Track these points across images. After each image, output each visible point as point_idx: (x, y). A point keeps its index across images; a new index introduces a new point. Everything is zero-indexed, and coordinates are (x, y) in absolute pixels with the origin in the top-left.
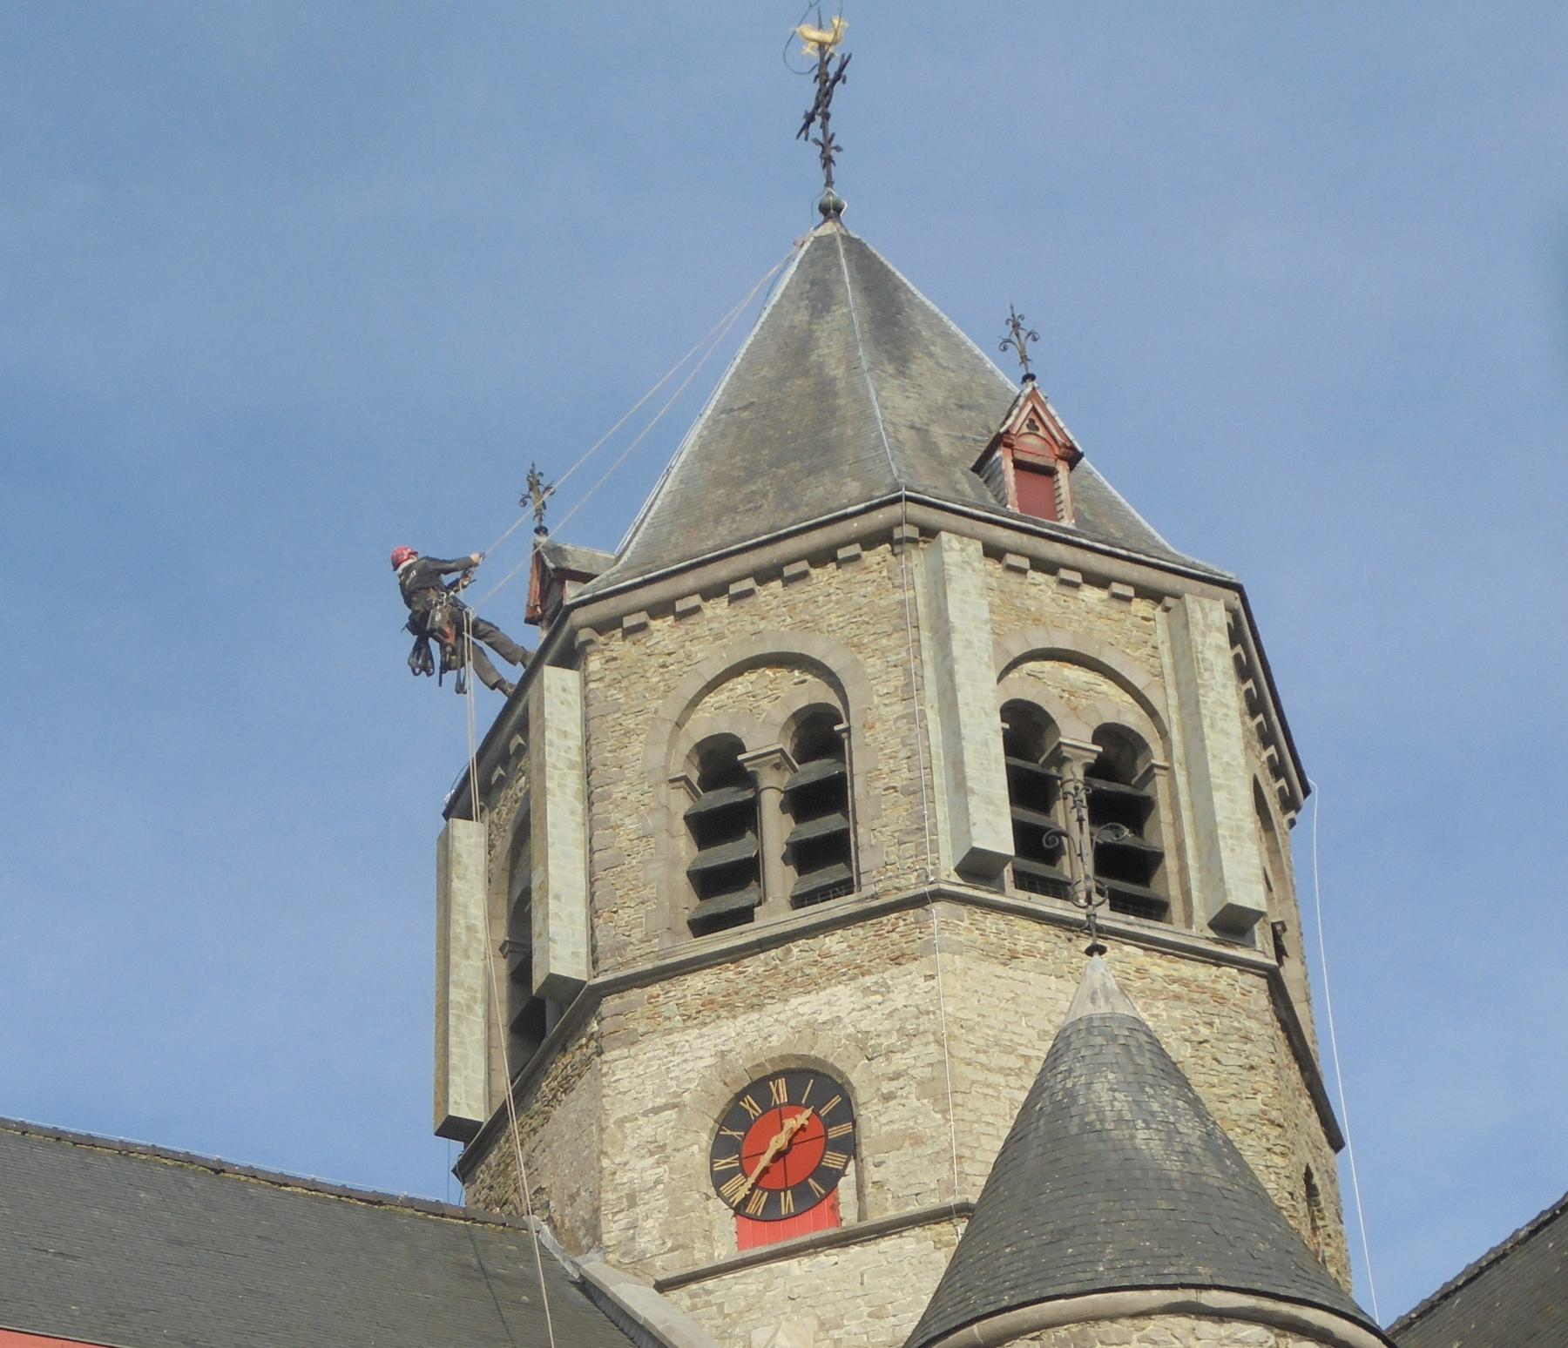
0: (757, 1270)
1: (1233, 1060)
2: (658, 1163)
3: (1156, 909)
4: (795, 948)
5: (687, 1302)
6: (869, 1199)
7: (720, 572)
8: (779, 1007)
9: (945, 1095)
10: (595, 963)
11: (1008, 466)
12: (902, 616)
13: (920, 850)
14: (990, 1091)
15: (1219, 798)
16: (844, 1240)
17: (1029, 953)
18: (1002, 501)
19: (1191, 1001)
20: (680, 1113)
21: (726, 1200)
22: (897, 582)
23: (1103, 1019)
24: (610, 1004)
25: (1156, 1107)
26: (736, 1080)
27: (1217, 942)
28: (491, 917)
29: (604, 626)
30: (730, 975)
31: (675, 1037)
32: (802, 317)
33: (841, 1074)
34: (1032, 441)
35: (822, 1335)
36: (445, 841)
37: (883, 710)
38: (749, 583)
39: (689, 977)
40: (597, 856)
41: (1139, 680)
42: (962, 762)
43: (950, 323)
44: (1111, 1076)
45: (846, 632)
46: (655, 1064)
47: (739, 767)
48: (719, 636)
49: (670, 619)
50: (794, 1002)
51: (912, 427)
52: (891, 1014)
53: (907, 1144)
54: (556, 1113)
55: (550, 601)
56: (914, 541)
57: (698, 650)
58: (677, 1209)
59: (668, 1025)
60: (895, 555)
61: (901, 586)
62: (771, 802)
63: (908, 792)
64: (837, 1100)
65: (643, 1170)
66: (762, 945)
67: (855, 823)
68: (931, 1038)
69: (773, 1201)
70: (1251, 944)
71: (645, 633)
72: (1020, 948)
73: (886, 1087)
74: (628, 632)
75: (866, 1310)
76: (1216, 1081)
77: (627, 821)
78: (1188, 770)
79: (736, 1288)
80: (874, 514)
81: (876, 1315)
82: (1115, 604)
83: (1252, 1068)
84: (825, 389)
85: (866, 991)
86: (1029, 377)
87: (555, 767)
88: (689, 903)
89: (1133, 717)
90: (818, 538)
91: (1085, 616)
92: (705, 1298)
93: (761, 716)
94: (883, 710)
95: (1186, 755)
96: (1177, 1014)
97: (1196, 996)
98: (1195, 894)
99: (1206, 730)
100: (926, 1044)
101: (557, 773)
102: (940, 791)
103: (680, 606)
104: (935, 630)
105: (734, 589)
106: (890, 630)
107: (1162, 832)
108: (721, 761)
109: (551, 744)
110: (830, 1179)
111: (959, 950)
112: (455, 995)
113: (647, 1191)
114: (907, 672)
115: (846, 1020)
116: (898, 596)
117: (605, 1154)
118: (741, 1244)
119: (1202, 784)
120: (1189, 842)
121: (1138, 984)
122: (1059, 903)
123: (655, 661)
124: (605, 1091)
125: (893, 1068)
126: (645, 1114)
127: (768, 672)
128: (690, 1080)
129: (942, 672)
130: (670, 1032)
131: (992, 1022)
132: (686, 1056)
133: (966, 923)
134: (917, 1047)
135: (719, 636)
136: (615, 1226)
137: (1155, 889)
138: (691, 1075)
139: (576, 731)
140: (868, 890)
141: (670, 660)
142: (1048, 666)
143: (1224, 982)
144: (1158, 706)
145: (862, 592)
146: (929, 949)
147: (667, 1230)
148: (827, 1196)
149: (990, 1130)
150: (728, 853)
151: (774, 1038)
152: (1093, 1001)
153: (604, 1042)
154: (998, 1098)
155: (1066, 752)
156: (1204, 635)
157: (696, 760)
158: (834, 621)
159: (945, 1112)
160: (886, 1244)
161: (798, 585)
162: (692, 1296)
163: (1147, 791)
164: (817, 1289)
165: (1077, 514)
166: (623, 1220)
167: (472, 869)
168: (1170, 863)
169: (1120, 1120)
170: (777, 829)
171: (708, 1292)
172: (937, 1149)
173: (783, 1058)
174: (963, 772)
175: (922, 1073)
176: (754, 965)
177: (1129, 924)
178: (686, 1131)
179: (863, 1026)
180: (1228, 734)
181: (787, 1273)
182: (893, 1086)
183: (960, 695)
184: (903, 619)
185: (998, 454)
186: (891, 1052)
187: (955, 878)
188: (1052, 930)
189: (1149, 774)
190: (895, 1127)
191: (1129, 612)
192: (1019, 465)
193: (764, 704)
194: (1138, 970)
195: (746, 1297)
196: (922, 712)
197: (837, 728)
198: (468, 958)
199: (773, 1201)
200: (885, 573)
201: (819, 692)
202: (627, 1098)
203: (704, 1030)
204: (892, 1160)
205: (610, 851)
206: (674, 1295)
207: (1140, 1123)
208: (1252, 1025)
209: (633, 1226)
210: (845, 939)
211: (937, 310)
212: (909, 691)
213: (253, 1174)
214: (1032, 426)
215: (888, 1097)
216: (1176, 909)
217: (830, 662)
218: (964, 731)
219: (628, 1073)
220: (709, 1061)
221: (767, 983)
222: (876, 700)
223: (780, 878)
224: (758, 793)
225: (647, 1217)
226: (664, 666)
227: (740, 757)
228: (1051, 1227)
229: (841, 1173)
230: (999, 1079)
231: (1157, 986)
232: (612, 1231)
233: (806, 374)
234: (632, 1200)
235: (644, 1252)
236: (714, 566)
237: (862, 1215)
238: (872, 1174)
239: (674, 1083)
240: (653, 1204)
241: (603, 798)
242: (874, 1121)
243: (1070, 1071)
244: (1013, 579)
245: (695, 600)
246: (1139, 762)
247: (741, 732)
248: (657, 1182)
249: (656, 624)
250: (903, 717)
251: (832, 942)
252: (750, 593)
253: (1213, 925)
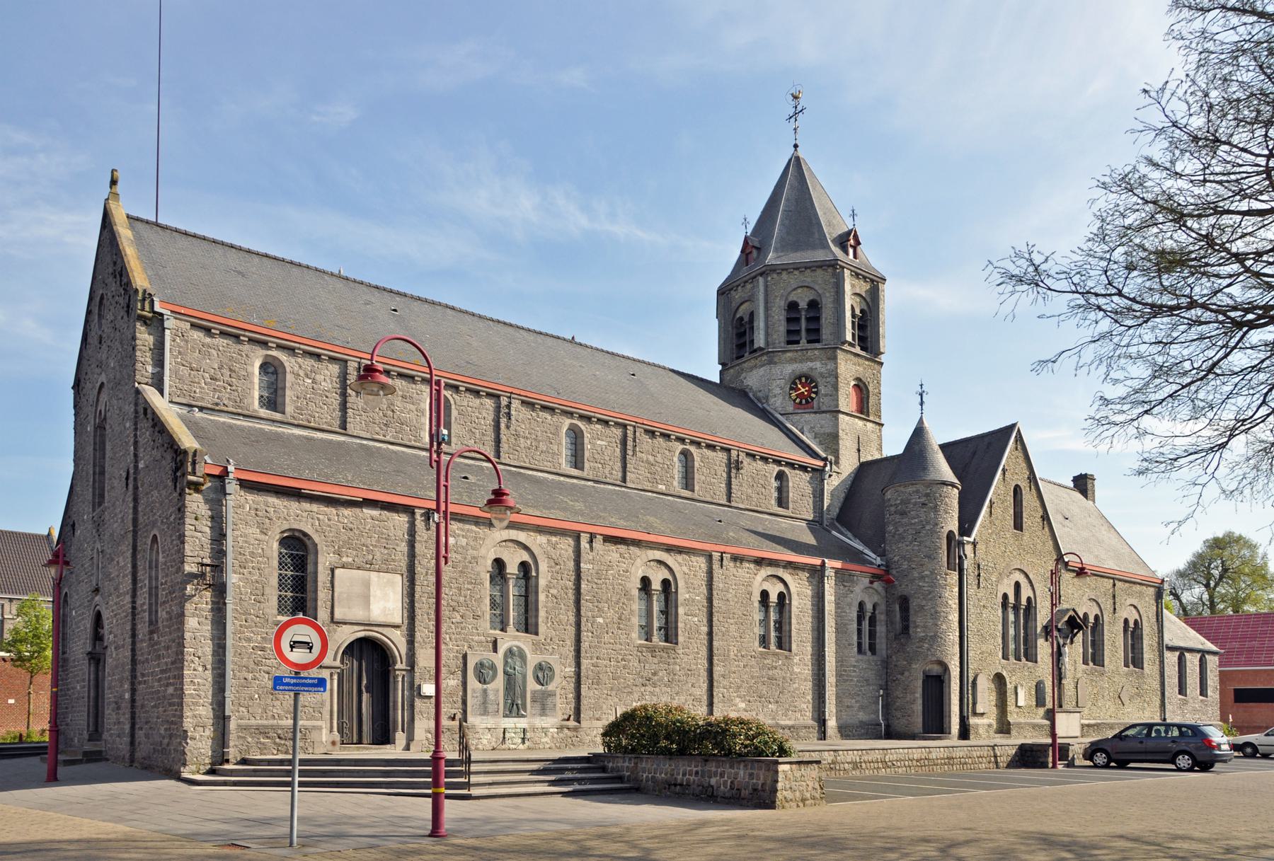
62: (803, 333)
108: (793, 306)
232: (772, 400)
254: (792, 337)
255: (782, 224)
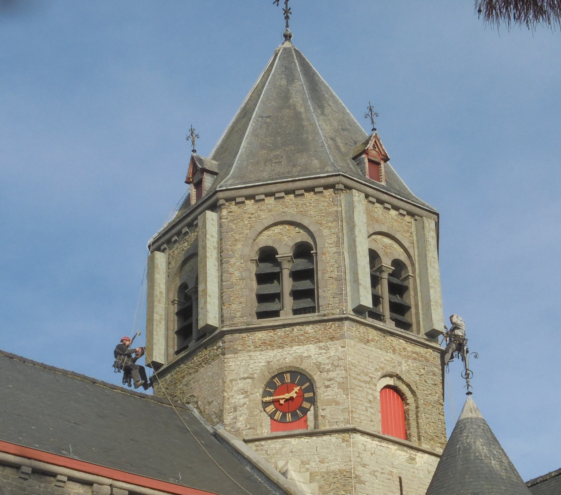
0: (280, 440)
1: (430, 382)
2: (245, 398)
3: (406, 326)
4: (296, 328)
5: (255, 448)
6: (320, 421)
7: (273, 188)
8: (289, 348)
9: (347, 389)
10: (222, 321)
11: (366, 161)
12: (337, 216)
13: (341, 302)
14: (361, 389)
15: (432, 291)
16: (311, 435)
17: (372, 340)
18: (364, 173)
19: (419, 360)
20: (253, 381)
21: (267, 413)
22: (336, 203)
23: (476, 419)
24: (228, 337)
25: (495, 452)
26: (273, 372)
27: (427, 340)
28: (168, 290)
29: (228, 200)
30: (272, 334)
31: (252, 353)
32: (284, 82)
33: (311, 376)
34: (374, 152)
35: (302, 466)
36: (151, 260)
37: (329, 249)
38: (282, 194)
39: (257, 333)
40: (224, 283)
41: (407, 244)
42: (357, 273)
43: (333, 91)
44: (481, 440)
45: (317, 218)
46: (244, 362)
47: (276, 259)
48: (270, 211)
49: (253, 201)
50: (295, 348)
51: (331, 139)
52: (329, 358)
53: (333, 404)
54: (202, 370)
55: (195, 177)
56: (342, 190)
57: (263, 215)
58: (251, 415)
59: (249, 348)
60: (335, 194)
61: (337, 205)
62: (286, 274)
63: (336, 279)
64: (308, 384)
65: (239, 399)
66: (284, 326)
67: (318, 288)
68: (343, 368)
69: (284, 416)
70: (436, 341)
71: (243, 205)
72: (370, 339)
73: (327, 383)
74: (237, 204)
75: (318, 460)
76: (425, 389)
77: (235, 272)
78: (420, 278)
79: (272, 446)
80: (329, 178)
81: (322, 462)
82: (400, 216)
83: (435, 385)
84: (297, 116)
85: (320, 348)
86: (374, 129)
87: (209, 248)
88: (254, 306)
89: (403, 257)
90: (309, 183)
91: (391, 219)
92: (261, 447)
93: (284, 241)
94: (329, 249)
95: (420, 273)
96: (415, 365)
97: (420, 359)
98: (421, 323)
99: (428, 266)
100: (341, 370)
101: (210, 250)
102: (346, 281)
103: (257, 198)
104: (348, 224)
105: (277, 195)
106: (332, 220)
107: (410, 299)
108: (268, 255)
109: (208, 240)
110: (305, 411)
111: (352, 338)
112: (156, 317)
113: (241, 407)
114: (338, 237)
115: (313, 357)
116: (335, 208)
117: (226, 391)
118: (272, 430)
119: (426, 287)
120: (420, 304)
121: (404, 353)
122: (381, 323)
123: (246, 216)
124: (226, 369)
125: (329, 377)
126: (240, 379)
127: (287, 226)
128: (257, 370)
129: (350, 240)
130: (250, 351)
131: (362, 364)
132: (255, 361)
133: (354, 329)
134: (338, 371)
135: (270, 211)
136: (229, 418)
137: (406, 318)
138: (257, 368)
139: (216, 235)
140: (322, 313)
141: (252, 216)
142: (379, 237)
143: (428, 354)
144: (412, 254)
145: (323, 204)
146: (342, 337)
147: (247, 421)
148: (303, 417)
149: (361, 402)
150: (270, 289)
151: (287, 359)
152: (471, 412)
153: (226, 351)
154: (363, 391)
155: (384, 269)
156: (428, 232)
157: (258, 253)
158: (312, 213)
159: (347, 395)
160: (325, 438)
161: (300, 198)
162: (257, 446)
163: (405, 283)
164: (301, 450)
165: (386, 181)
166: (232, 416)
167: (162, 270)
168: (413, 310)
169: (486, 456)
170: (288, 284)
171: (262, 446)
172: (344, 407)
173: (290, 367)
174: (358, 277)
175: (340, 380)
176: (280, 332)
177: (402, 332)
178: (255, 388)
179: (319, 360)
180: (435, 268)
181: (290, 443)
182: (329, 383)
183: (357, 249)
184: (337, 217)
185: (363, 156)
186: (328, 371)
187: (352, 313)
188: (379, 333)
189: (407, 278)
190: (330, 397)
191: (404, 220)
192: (370, 161)
193: (285, 238)
194: (404, 348)
195: (276, 449)
196: (343, 252)
197: (312, 252)
198: (160, 303)
199: (284, 416)
200: (331, 199)
201: (306, 238)
202: (234, 372)
203: (262, 353)
204: (328, 409)
205: (229, 282)
206: (250, 445)
207: (492, 459)
208: (435, 369)
209: (235, 418)
210: (313, 329)
211: (328, 85)
212: (338, 243)
213: (104, 384)
214: (374, 146)
215: (327, 387)
216: (414, 327)
217: (311, 228)
218: (359, 262)
219: (233, 364)
220: (263, 364)
221: (285, 339)
222: (327, 244)
223: (288, 301)
224: (281, 269)
225: (240, 416)
226: (250, 218)
227: (276, 256)
228: (471, 491)
229: (309, 410)
230: (363, 384)
231: (409, 354)
232: (228, 418)
233: (289, 107)
234: (235, 409)
235: (239, 428)
236: (271, 186)
237: (316, 426)
238: (321, 413)
239: (251, 370)
240: (243, 411)
241: (228, 262)
242: (323, 394)
243: (468, 436)
244: (370, 205)
245: (263, 197)
246: (403, 272)
247: (276, 246)
248: (244, 404)
249: (247, 202)
250: (336, 253)
251: (309, 329)
252: (283, 197)
253: (426, 334)
254: (267, 304)
255: (255, 134)
